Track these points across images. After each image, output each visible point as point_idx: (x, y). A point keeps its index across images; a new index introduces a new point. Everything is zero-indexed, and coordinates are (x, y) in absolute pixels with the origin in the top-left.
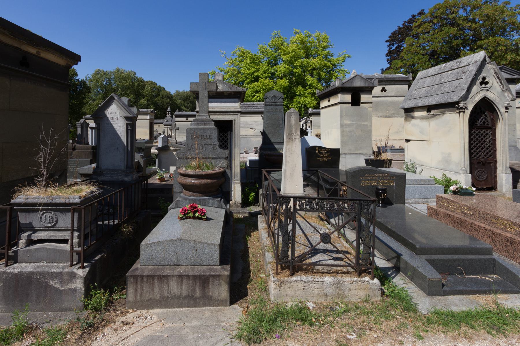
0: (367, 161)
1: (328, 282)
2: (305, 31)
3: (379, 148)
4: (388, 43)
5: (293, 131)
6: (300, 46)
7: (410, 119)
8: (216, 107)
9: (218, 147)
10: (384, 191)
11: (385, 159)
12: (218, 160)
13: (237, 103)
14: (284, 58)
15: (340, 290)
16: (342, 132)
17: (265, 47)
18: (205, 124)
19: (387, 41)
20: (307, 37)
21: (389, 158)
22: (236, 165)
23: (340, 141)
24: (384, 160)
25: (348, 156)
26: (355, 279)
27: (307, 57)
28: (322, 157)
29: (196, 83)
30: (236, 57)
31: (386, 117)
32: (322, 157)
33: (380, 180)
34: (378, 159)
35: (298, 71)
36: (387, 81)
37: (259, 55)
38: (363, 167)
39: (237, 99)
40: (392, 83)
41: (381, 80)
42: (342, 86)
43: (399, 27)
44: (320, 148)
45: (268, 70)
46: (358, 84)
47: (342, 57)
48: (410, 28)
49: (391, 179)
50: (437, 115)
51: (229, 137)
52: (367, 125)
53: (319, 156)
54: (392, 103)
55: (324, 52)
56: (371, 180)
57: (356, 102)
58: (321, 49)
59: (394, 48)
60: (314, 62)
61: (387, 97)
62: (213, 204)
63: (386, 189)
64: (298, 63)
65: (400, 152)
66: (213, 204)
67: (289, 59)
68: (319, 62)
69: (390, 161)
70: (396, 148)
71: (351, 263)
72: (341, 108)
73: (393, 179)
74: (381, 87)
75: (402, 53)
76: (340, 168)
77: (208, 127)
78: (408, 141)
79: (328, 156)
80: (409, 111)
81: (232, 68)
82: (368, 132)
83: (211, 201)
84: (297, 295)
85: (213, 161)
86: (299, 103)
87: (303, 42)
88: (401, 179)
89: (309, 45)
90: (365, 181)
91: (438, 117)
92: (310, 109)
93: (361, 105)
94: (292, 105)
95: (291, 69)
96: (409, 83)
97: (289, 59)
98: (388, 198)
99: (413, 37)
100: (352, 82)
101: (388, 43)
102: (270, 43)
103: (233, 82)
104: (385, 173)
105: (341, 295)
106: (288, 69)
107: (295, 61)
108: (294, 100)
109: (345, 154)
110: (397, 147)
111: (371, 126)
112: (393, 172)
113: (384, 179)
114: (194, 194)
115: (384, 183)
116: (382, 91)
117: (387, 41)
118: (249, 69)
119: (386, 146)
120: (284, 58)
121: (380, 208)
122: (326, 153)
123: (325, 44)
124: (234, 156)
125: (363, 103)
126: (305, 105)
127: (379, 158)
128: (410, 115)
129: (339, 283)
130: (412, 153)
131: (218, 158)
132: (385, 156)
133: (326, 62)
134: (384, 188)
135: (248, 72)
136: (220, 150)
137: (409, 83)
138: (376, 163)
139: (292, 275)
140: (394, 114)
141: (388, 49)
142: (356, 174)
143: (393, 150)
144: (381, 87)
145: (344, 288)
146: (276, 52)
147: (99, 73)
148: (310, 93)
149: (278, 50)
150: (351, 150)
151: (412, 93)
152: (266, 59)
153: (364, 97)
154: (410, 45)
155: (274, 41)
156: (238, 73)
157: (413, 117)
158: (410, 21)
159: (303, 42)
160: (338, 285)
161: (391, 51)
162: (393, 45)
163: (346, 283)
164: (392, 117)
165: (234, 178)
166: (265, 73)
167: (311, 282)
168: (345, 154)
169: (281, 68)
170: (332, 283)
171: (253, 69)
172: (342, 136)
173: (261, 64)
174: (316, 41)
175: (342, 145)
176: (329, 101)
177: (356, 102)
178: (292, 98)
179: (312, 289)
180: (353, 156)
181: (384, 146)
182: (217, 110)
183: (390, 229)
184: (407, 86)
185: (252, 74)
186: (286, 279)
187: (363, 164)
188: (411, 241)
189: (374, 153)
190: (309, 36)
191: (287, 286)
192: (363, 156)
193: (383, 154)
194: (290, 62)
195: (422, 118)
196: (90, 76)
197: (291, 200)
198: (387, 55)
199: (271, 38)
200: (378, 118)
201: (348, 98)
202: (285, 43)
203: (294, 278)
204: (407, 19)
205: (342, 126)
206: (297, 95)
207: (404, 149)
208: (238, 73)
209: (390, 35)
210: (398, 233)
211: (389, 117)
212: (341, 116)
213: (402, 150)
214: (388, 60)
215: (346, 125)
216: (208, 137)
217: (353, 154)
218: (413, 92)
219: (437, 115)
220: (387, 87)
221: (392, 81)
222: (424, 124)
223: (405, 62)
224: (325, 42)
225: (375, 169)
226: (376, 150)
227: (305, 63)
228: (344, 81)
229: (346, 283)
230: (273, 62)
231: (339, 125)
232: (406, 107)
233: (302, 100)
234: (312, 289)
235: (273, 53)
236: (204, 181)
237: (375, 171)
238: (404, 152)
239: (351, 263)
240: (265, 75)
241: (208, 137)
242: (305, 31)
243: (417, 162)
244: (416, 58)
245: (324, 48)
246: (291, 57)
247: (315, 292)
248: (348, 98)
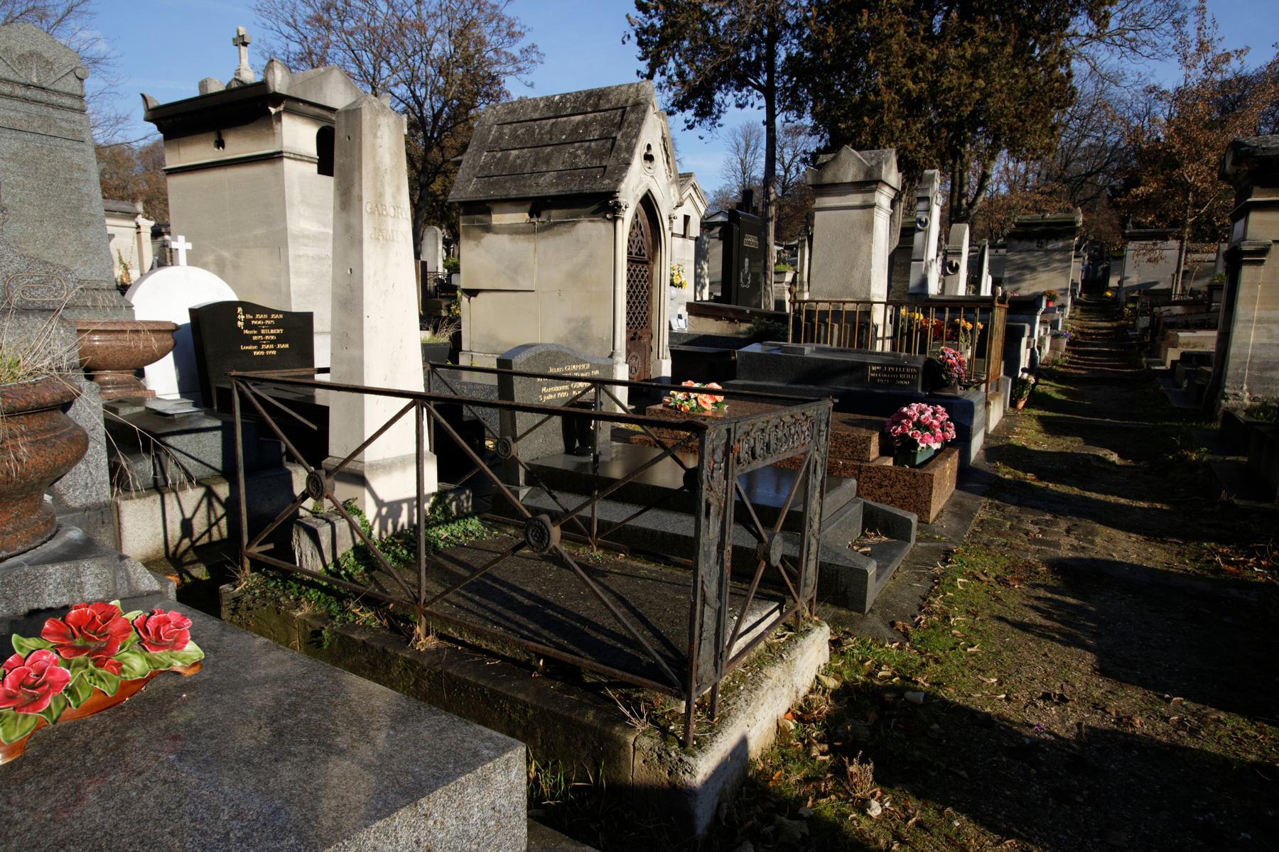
7: (477, 232)
32: (258, 343)
50: (556, 224)
71: (644, 637)
91: (562, 228)
122: (271, 327)
157: (488, 229)
176: (220, 144)
185: (1103, 78)
195: (514, 230)
197: (401, 509)
206: (834, 147)
219: (556, 224)
222: (522, 245)
239: (644, 637)
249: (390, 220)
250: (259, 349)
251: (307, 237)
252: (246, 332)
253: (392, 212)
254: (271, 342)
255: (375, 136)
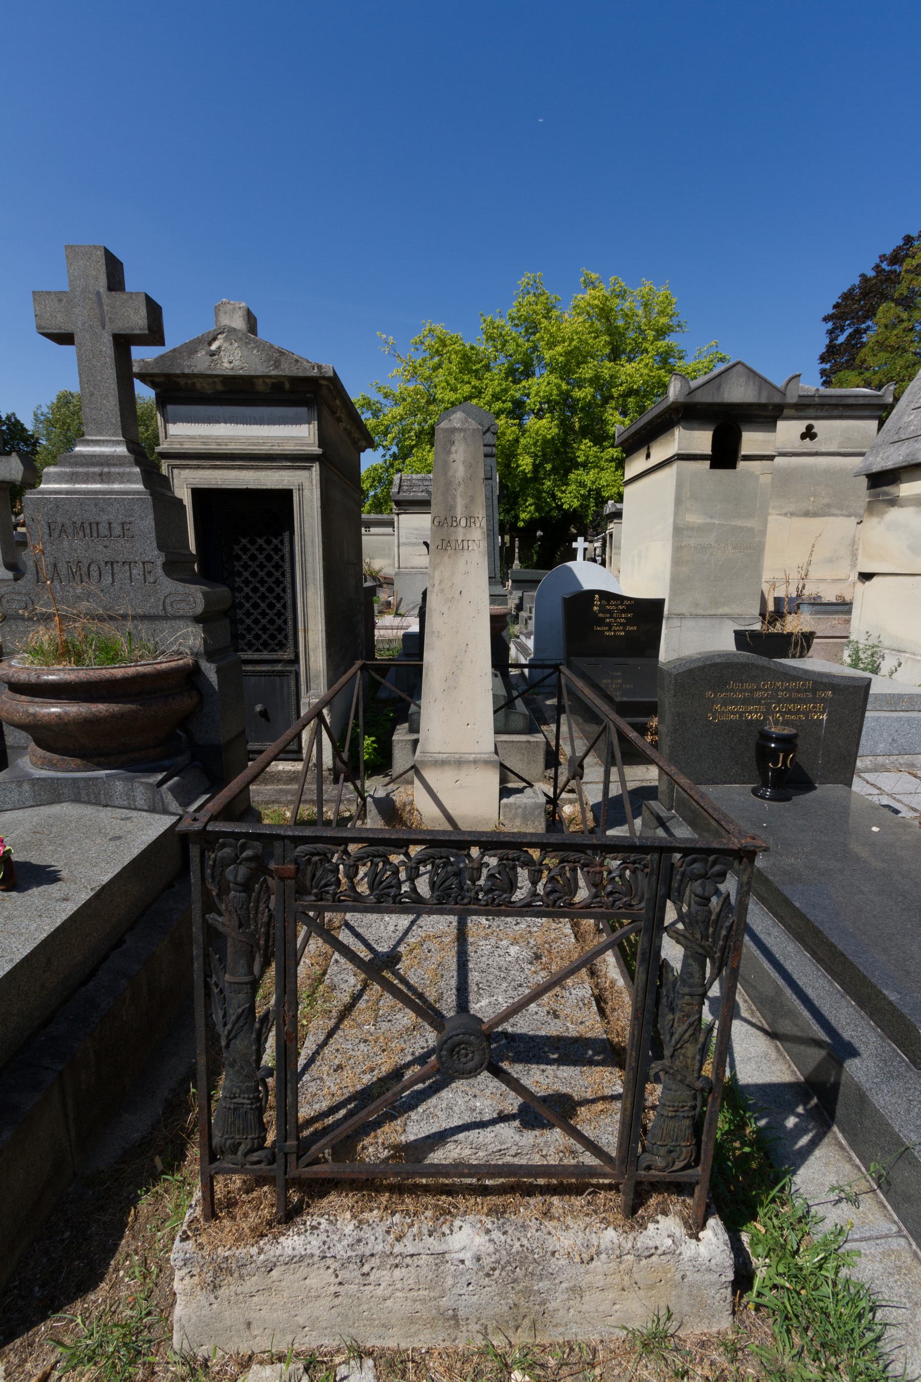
0: (739, 636)
1: (467, 1256)
2: (612, 279)
3: (778, 601)
4: (830, 325)
5: (459, 511)
6: (598, 325)
7: (882, 506)
8: (232, 439)
9: (159, 571)
10: (788, 743)
11: (795, 631)
12: (166, 625)
13: (305, 427)
14: (547, 355)
15: (528, 1292)
16: (677, 549)
17: (499, 322)
18: (102, 478)
19: (826, 319)
20: (618, 296)
21: (806, 629)
22: (311, 645)
23: (668, 577)
24: (790, 635)
25: (689, 623)
26: (610, 1235)
27: (615, 355)
28: (610, 626)
29: (59, 296)
30: (424, 355)
31: (807, 514)
32: (610, 626)
33: (779, 702)
34: (772, 630)
35: (584, 393)
36: (822, 406)
37: (484, 348)
38: (727, 654)
39: (303, 410)
40: (835, 413)
41: (806, 401)
42: (688, 400)
43: (863, 276)
44: (607, 596)
45: (505, 391)
46: (738, 392)
47: (706, 361)
48: (891, 279)
49: (814, 700)
51: (286, 550)
52: (751, 530)
53: (601, 622)
54: (828, 473)
55: (659, 343)
56: (745, 702)
57: (725, 455)
58: (651, 334)
59: (841, 339)
60: (632, 372)
61: (816, 454)
62: (130, 796)
63: (795, 736)
64: (587, 372)
65: (842, 612)
66: (130, 796)
67: (561, 359)
68: (646, 371)
69: (808, 637)
70: (824, 600)
72: (678, 474)
73: (822, 700)
74: (800, 426)
75: (864, 350)
76: (660, 659)
77: (116, 486)
78: (866, 577)
79: (629, 622)
80: (882, 480)
81: (411, 388)
82: (753, 550)
83: (119, 786)
84: (301, 1320)
85: (144, 628)
86: (582, 484)
87: (605, 313)
88: (852, 697)
89: (620, 323)
90: (725, 703)
92: (610, 502)
93: (741, 464)
94: (564, 492)
95: (564, 387)
96: (880, 412)
97: (561, 359)
98: (797, 766)
99: (898, 302)
100: (719, 387)
101: (830, 325)
102: (513, 311)
103: (416, 426)
104: (795, 678)
105: (528, 1313)
106: (558, 387)
107: (578, 364)
108: (572, 476)
109: (681, 616)
110: (829, 596)
111: (764, 532)
112: (821, 674)
113: (791, 701)
114: (56, 757)
115: (789, 712)
116: (803, 436)
117: (826, 319)
118: (454, 390)
119: (799, 596)
120: (547, 355)
121: (766, 804)
122: (623, 611)
123: (664, 320)
124: (305, 615)
125: (747, 458)
126: (598, 491)
127: (778, 628)
128: (887, 494)
129: (521, 1259)
130: (878, 615)
131: (166, 618)
132: (793, 624)
133: (662, 372)
134: (787, 731)
135: (453, 396)
136: (169, 585)
137: (880, 412)
138: (769, 643)
139: (289, 1216)
140: (828, 506)
141: (827, 341)
142: (709, 673)
143: (819, 606)
144: (800, 426)
145: (543, 1285)
146: (528, 341)
147: (68, 402)
148: (612, 460)
149: (534, 333)
150: (697, 605)
151: (902, 424)
152: (501, 358)
153: (752, 441)
154: (886, 326)
155: (521, 304)
156: (429, 403)
157: (893, 502)
158: (896, 258)
159: (605, 313)
160: (517, 1270)
161: (834, 346)
162: (842, 330)
163: (556, 1264)
164: (824, 516)
165: (308, 689)
166: (498, 399)
167: (375, 1262)
168: (681, 616)
169: (541, 385)
170: (487, 1261)
171: (467, 389)
172: (676, 561)
173: (488, 375)
174: (640, 312)
175: (673, 591)
177: (725, 455)
178: (568, 471)
179: (379, 1291)
180: (702, 622)
181: (794, 595)
182: (233, 448)
183: (798, 914)
184: (874, 424)
186: (241, 1252)
187: (728, 644)
188: (893, 997)
189: (762, 615)
190: (622, 295)
191: (251, 1284)
192: (730, 622)
193: (789, 618)
194: (563, 368)
196: (45, 410)
198: (823, 359)
199: (516, 297)
200: (785, 519)
201: (702, 440)
202: (555, 313)
203: (292, 1242)
204: (888, 251)
205: (678, 531)
207: (851, 604)
208: (429, 403)
209: (836, 299)
210: (834, 940)
211: (815, 515)
212: (678, 501)
213: (844, 607)
214: (823, 373)
215: (691, 528)
216: (117, 530)
217: (704, 616)
218: (906, 419)
220: (820, 426)
221: (836, 406)
223: (867, 374)
224: (661, 313)
225: (762, 661)
226: (771, 607)
227: (606, 374)
228: (694, 384)
229: (556, 1264)
230: (522, 370)
231: (671, 529)
232: (876, 468)
233: (589, 478)
234: (379, 1291)
235: (521, 341)
236: (74, 709)
237: (763, 668)
238: (849, 612)
240: (498, 405)
241: (117, 530)
242: (612, 279)
243: (886, 643)
244: (900, 362)
245: (661, 333)
246: (568, 354)
247: (399, 1305)
248: (702, 440)
249: (460, 529)
250: (610, 630)
251: (692, 529)
252: (601, 615)
253: (463, 523)
254: (621, 624)
255: (449, 452)
